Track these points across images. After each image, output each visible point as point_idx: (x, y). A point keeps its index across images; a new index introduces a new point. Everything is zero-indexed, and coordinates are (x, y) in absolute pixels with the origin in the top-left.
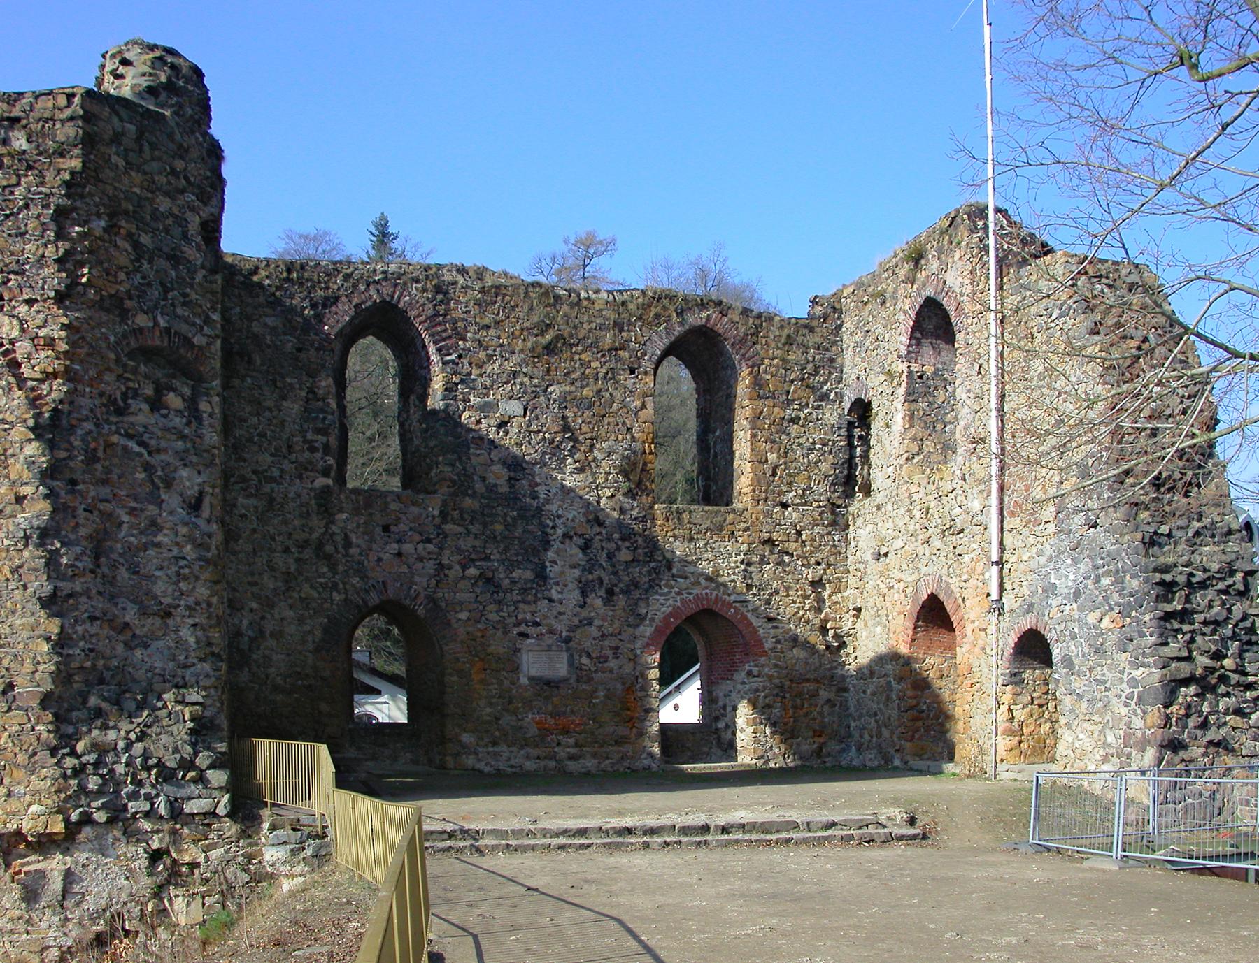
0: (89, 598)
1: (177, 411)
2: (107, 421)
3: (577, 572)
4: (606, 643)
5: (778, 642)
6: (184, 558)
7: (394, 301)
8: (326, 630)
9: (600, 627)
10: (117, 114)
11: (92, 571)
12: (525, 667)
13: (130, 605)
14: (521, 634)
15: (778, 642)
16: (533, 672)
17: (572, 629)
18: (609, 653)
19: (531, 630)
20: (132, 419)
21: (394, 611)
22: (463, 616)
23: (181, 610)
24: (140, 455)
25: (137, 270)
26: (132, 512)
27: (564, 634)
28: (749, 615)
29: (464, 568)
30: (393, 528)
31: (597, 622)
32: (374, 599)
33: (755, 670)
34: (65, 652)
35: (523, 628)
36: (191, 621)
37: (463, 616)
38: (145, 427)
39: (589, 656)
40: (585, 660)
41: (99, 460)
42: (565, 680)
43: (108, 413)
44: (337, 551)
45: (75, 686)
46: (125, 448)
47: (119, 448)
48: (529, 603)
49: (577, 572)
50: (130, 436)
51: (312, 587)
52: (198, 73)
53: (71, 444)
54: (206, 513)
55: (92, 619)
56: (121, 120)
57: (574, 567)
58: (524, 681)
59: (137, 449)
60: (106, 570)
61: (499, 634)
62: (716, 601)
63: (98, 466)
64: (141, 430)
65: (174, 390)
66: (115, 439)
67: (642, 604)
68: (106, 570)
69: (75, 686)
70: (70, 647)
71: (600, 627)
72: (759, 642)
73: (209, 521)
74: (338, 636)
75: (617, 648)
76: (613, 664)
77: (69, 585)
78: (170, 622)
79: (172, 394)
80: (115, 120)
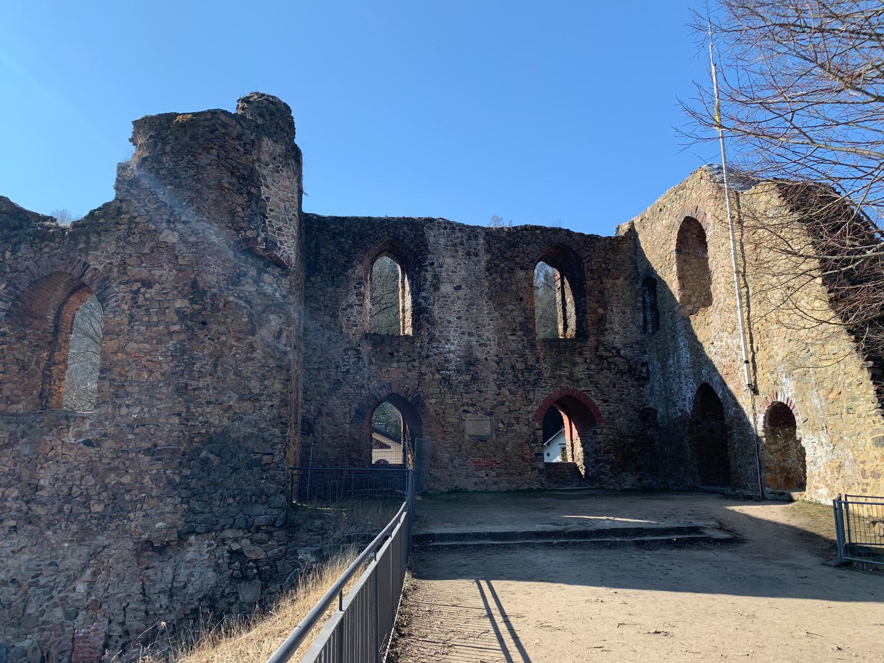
0: (208, 390)
1: (269, 283)
2: (228, 289)
3: (495, 376)
4: (513, 415)
5: (610, 414)
6: (268, 367)
7: (484, 583)
8: (357, 411)
9: (508, 407)
10: (240, 124)
11: (211, 375)
12: (467, 430)
13: (233, 394)
14: (465, 411)
15: (610, 414)
16: (472, 433)
17: (494, 407)
18: (514, 421)
19: (470, 409)
20: (244, 288)
21: (398, 400)
22: (433, 401)
23: (264, 397)
24: (245, 308)
25: (249, 207)
26: (239, 340)
27: (489, 410)
28: (592, 398)
29: (433, 374)
30: (395, 354)
31: (507, 404)
32: (384, 393)
33: (598, 431)
34: (190, 423)
35: (465, 408)
36: (270, 403)
37: (433, 401)
38: (250, 292)
39: (503, 423)
40: (501, 425)
41: (220, 310)
42: (490, 436)
43: (228, 284)
44: (364, 367)
45: (195, 444)
46: (237, 304)
47: (233, 304)
48: (469, 393)
49: (495, 376)
50: (240, 298)
51: (350, 387)
52: (288, 109)
53: (203, 301)
54: (284, 341)
55: (209, 403)
56: (243, 128)
57: (493, 373)
58: (467, 438)
59: (243, 304)
60: (221, 375)
61: (453, 411)
62: (573, 391)
63: (220, 314)
64: (247, 294)
65: (268, 273)
66: (231, 299)
67: (531, 393)
68: (221, 375)
69: (195, 444)
70: (193, 420)
71: (508, 407)
72: (599, 414)
73: (285, 345)
74: (365, 412)
75: (518, 418)
76: (516, 427)
77: (196, 383)
78: (257, 404)
79: (266, 275)
80: (238, 126)
